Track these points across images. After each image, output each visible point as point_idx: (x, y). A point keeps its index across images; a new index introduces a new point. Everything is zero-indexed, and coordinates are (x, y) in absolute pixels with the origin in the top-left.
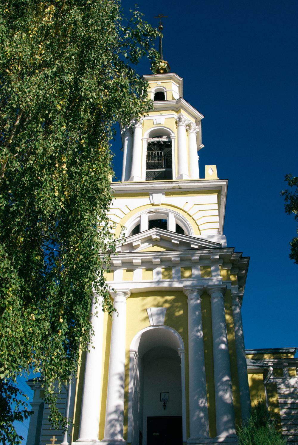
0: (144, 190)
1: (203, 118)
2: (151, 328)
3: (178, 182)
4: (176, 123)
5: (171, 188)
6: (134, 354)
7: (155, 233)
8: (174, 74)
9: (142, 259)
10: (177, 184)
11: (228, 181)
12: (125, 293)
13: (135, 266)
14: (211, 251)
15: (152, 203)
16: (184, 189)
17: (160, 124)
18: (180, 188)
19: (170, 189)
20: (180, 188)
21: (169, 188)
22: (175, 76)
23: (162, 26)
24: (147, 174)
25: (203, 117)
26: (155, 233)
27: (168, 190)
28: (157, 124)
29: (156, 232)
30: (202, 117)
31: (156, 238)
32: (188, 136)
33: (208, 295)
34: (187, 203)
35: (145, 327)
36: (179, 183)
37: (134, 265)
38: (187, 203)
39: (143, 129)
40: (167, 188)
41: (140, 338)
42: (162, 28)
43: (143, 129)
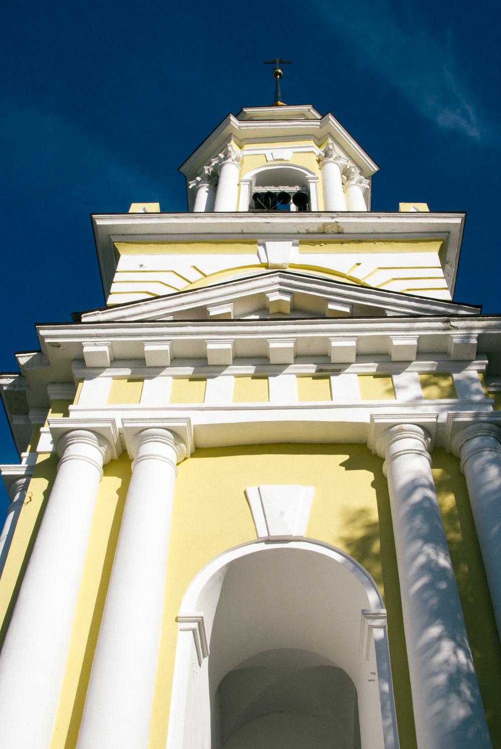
0: (242, 233)
1: (376, 169)
2: (263, 547)
3: (334, 215)
4: (319, 161)
5: (315, 229)
6: (194, 631)
7: (278, 287)
8: (310, 107)
9: (235, 343)
10: (333, 218)
11: (466, 216)
12: (177, 436)
13: (212, 366)
14: (453, 324)
15: (264, 261)
16: (350, 236)
17: (282, 160)
18: (338, 233)
19: (314, 233)
20: (338, 233)
21: (311, 230)
22: (312, 111)
23: (280, 71)
24: (256, 196)
25: (376, 169)
26: (278, 287)
27: (309, 236)
28: (275, 160)
29: (281, 284)
30: (374, 168)
31: (280, 301)
32: (344, 192)
33: (451, 454)
34: (358, 264)
35: (239, 543)
36: (337, 217)
37: (210, 363)
38: (358, 264)
39: (241, 169)
40: (303, 231)
41: (220, 585)
42: (280, 74)
43: (241, 169)
